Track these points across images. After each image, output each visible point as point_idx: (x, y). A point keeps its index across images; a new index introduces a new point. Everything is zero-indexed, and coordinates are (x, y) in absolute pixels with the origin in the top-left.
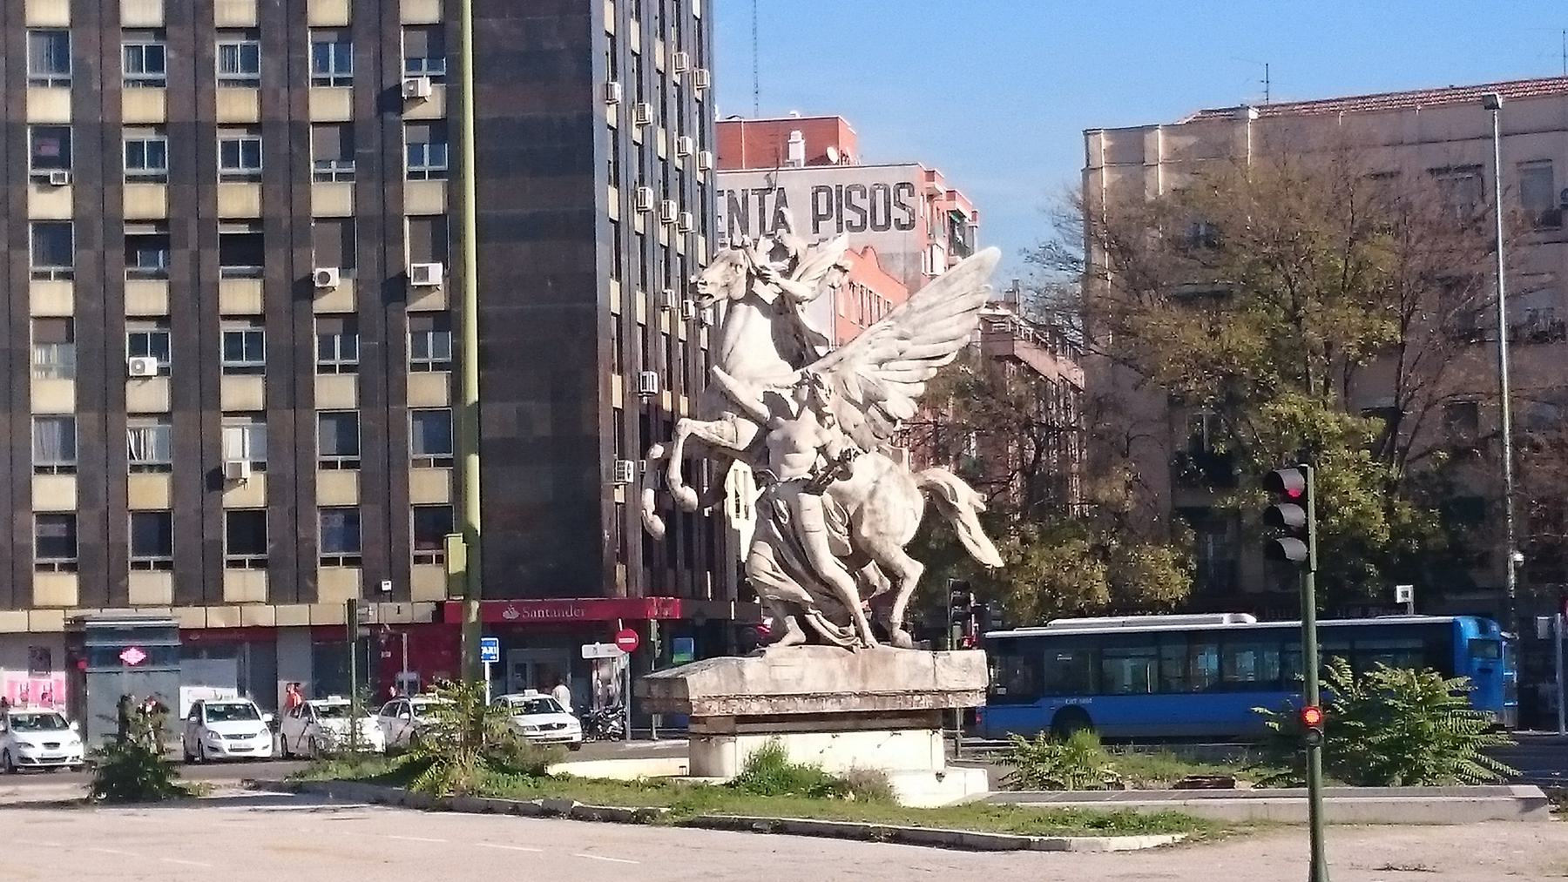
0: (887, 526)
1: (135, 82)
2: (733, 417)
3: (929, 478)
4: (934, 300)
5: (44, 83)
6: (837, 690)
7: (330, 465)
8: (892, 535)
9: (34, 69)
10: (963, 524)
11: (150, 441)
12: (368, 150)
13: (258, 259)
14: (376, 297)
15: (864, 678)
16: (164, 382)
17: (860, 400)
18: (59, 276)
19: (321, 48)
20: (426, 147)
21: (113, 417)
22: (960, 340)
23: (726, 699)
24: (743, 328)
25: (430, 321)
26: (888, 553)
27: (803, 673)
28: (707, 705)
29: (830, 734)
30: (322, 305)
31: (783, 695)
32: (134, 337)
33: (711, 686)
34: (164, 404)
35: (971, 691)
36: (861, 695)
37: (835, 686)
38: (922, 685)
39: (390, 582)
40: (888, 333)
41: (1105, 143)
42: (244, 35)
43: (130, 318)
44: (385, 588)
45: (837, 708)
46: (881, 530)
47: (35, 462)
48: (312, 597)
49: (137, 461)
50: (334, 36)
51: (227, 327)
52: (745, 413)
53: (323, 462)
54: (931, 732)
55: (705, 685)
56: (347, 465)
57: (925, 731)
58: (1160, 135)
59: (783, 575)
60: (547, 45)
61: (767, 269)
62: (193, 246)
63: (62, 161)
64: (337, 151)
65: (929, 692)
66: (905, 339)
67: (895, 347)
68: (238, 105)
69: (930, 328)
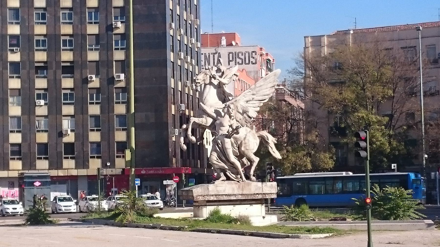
0: (249, 147)
1: (38, 23)
2: (206, 117)
3: (261, 134)
4: (262, 84)
5: (12, 23)
6: (235, 193)
7: (93, 130)
8: (250, 150)
9: (10, 19)
10: (270, 147)
11: (42, 124)
12: (103, 42)
13: (72, 73)
14: (105, 83)
15: (243, 190)
16: (46, 107)
17: (241, 112)
18: (17, 77)
19: (90, 13)
20: (120, 41)
21: (32, 117)
22: (269, 95)
23: (204, 196)
24: (209, 92)
25: (121, 90)
26: (249, 155)
27: (225, 188)
28: (198, 197)
29: (233, 206)
30: (90, 85)
31: (220, 195)
32: (37, 94)
33: (200, 192)
34: (46, 113)
35: (273, 193)
36: (241, 195)
37: (234, 192)
38: (259, 192)
39: (109, 163)
40: (249, 93)
41: (310, 40)
42: (68, 10)
43: (37, 89)
44: (108, 165)
45: (235, 198)
46: (247, 149)
47: (10, 129)
48: (88, 167)
49: (38, 129)
50: (94, 10)
51: (64, 92)
52: (209, 116)
53: (91, 129)
54: (261, 205)
55: (198, 192)
56: (97, 130)
57: (260, 205)
58: (325, 38)
59: (220, 161)
60: (153, 13)
61: (215, 75)
62: (54, 69)
63: (18, 45)
64: (95, 42)
65: (261, 194)
66: (254, 95)
67: (251, 97)
68: (67, 29)
69: (261, 92)
